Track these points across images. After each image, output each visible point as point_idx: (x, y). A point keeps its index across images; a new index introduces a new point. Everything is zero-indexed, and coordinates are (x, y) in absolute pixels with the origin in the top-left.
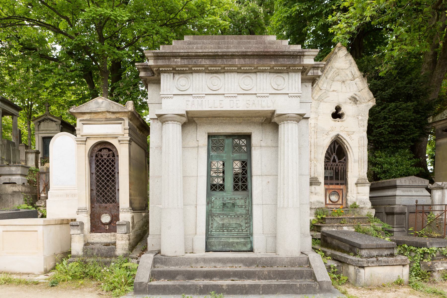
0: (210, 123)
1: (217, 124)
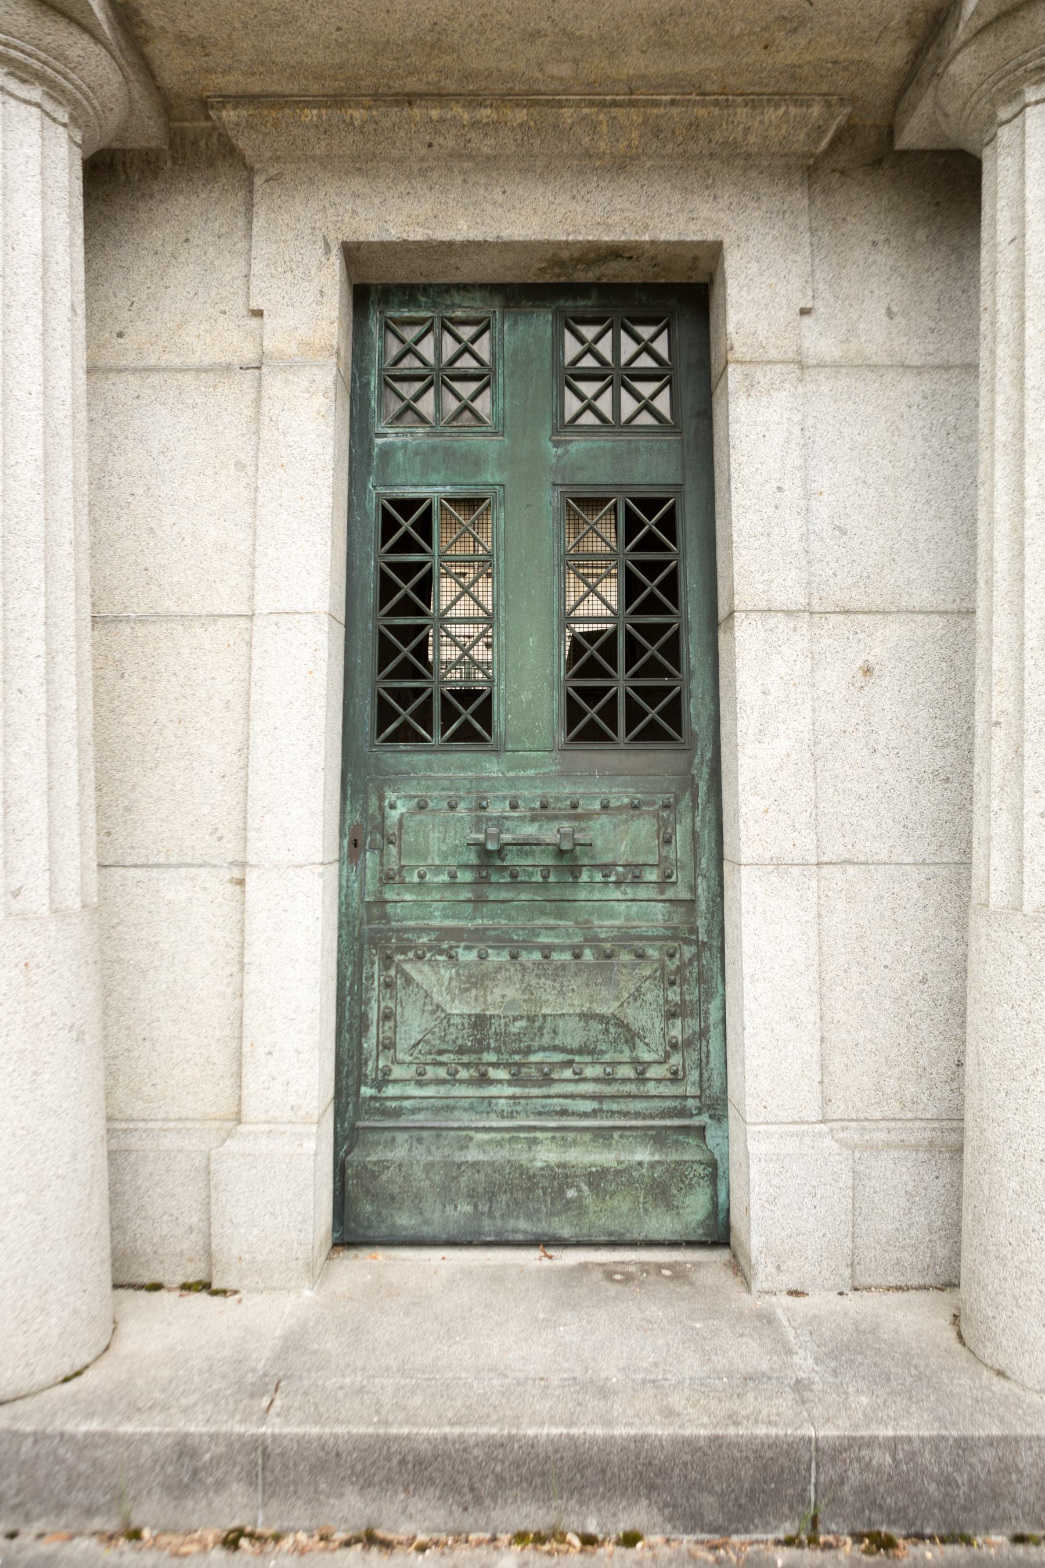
0: (365, 164)
1: (424, 173)
